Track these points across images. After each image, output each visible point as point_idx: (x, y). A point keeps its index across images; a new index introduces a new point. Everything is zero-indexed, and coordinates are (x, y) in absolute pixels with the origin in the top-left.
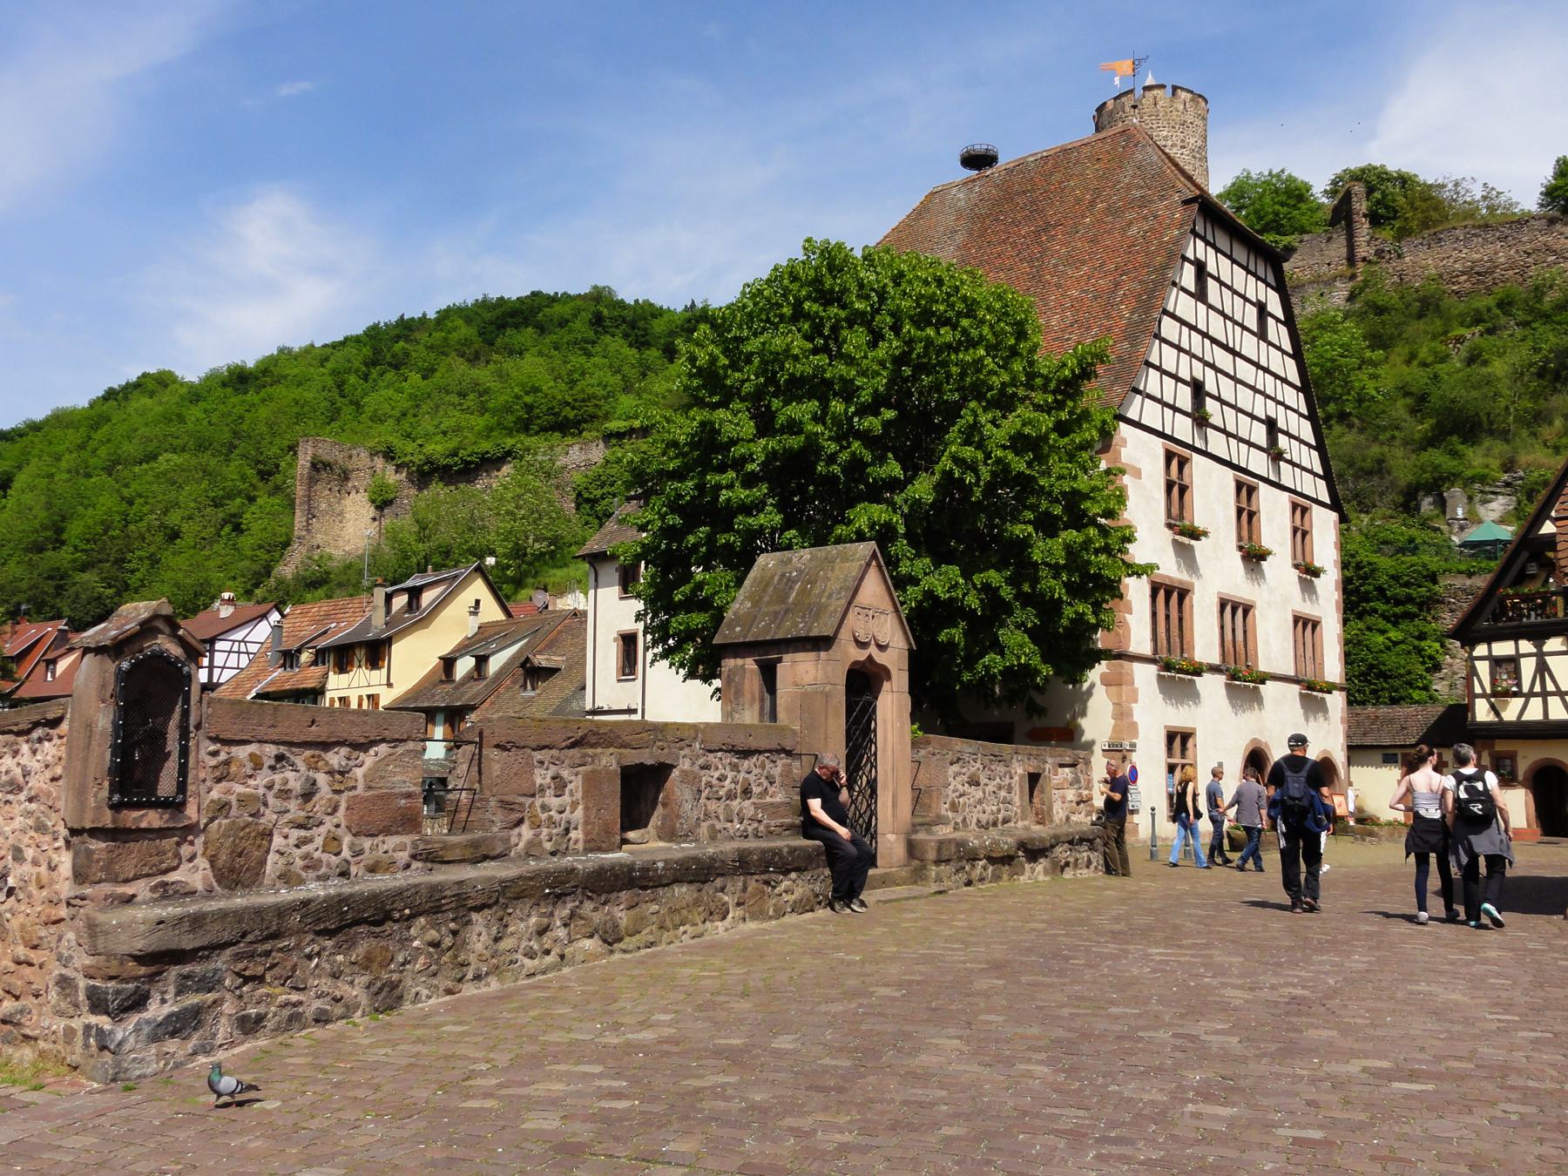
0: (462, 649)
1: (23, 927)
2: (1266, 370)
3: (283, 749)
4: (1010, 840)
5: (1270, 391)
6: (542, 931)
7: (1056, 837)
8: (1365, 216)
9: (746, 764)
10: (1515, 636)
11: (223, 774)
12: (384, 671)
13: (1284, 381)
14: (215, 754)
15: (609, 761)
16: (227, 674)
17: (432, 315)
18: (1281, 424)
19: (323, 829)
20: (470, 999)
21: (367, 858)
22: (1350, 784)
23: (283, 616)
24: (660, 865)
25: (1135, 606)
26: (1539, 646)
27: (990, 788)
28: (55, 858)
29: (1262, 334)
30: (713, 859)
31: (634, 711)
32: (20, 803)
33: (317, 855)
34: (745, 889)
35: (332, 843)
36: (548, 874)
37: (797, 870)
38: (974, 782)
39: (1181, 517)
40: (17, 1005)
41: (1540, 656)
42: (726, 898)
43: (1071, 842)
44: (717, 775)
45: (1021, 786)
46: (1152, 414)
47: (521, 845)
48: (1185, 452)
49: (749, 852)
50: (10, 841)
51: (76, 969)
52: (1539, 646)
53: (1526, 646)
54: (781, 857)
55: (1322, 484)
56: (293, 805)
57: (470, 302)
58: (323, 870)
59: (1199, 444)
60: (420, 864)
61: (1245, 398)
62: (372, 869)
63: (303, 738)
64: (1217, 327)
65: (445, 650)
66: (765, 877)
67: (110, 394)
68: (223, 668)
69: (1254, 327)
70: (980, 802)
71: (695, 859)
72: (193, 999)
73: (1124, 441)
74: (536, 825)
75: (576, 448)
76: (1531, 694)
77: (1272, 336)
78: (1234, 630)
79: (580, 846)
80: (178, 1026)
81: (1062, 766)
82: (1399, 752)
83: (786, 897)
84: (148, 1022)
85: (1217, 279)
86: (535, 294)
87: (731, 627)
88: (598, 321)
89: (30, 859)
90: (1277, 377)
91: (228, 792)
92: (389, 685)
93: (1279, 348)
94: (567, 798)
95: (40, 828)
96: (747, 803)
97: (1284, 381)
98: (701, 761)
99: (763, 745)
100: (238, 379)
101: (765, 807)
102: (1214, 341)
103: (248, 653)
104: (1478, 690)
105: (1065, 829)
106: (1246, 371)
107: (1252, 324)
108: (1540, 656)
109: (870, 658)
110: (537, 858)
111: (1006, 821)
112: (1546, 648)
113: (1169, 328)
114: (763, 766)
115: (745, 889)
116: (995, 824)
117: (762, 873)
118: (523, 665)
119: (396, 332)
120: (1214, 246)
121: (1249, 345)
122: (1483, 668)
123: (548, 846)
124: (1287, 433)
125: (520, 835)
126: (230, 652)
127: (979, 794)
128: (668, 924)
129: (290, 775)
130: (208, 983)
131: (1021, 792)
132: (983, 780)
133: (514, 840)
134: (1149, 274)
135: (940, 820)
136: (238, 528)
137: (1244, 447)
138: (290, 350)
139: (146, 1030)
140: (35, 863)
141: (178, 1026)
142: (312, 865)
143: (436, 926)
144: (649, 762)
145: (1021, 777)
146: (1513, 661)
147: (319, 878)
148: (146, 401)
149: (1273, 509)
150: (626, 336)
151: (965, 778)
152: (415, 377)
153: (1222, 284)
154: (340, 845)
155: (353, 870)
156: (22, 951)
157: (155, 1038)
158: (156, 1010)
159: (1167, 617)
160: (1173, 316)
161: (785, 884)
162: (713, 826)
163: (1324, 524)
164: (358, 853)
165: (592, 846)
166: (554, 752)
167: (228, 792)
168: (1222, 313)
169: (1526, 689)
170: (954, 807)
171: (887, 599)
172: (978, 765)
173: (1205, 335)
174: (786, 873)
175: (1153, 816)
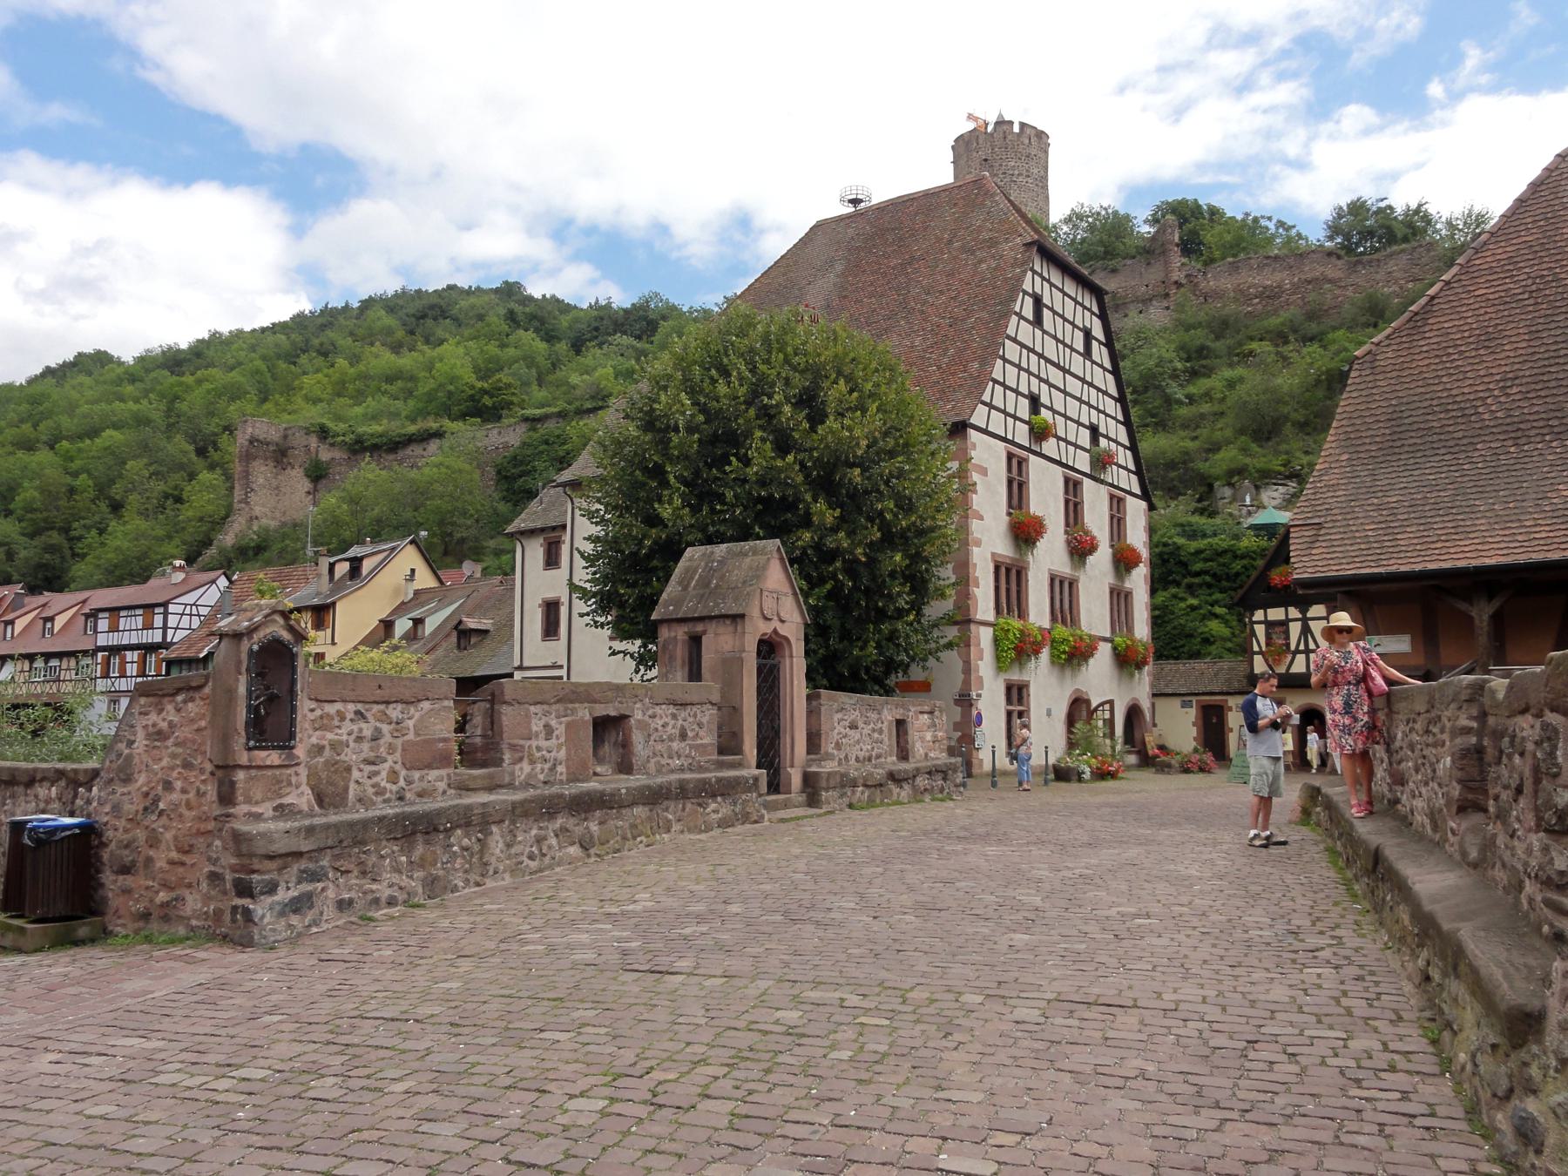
0: (401, 609)
1: (176, 838)
2: (1091, 385)
3: (360, 707)
4: (881, 771)
5: (1093, 402)
6: (539, 840)
7: (918, 769)
8: (1177, 245)
9: (683, 714)
10: (1285, 605)
11: (323, 724)
12: (329, 631)
13: (1105, 393)
14: (312, 710)
15: (585, 713)
16: (180, 635)
17: (356, 305)
18: (1102, 430)
19: (386, 766)
20: (493, 889)
21: (417, 786)
22: (1155, 725)
23: (231, 582)
24: (623, 791)
25: (981, 582)
26: (1304, 611)
27: (866, 731)
28: (203, 788)
29: (1087, 353)
30: (661, 787)
31: (561, 667)
32: (167, 747)
33: (383, 784)
34: (684, 809)
35: (393, 776)
36: (544, 798)
37: (722, 795)
38: (853, 726)
39: (1020, 507)
40: (173, 895)
41: (1305, 621)
42: (670, 817)
43: (929, 773)
44: (660, 723)
45: (890, 730)
46: (997, 423)
47: (523, 777)
48: (1024, 454)
49: (688, 781)
50: (159, 776)
51: (223, 867)
52: (1304, 611)
53: (1294, 612)
54: (710, 785)
55: (1134, 478)
56: (366, 746)
57: (390, 293)
58: (388, 795)
59: (1035, 448)
60: (453, 791)
61: (1073, 408)
62: (420, 795)
63: (372, 699)
64: (1051, 349)
65: (384, 614)
66: (700, 800)
67: (48, 371)
68: (176, 629)
69: (1081, 349)
70: (858, 742)
71: (649, 787)
72: (306, 887)
73: (974, 446)
74: (532, 762)
75: (495, 432)
76: (1297, 651)
77: (1096, 357)
78: (1061, 600)
79: (564, 777)
80: (298, 905)
81: (921, 713)
82: (1194, 699)
83: (714, 816)
84: (278, 903)
85: (1051, 309)
86: (451, 288)
87: (666, 606)
88: (511, 317)
89: (178, 788)
90: (1099, 390)
91: (323, 738)
92: (333, 643)
93: (1101, 366)
94: (554, 741)
95: (187, 765)
96: (683, 745)
97: (1105, 393)
98: (650, 712)
99: (695, 699)
100: (173, 361)
101: (697, 747)
102: (1048, 361)
103: (199, 615)
104: (1256, 648)
105: (924, 764)
106: (1074, 386)
107: (1079, 345)
108: (1305, 621)
109: (775, 631)
110: (534, 787)
111: (878, 757)
112: (1309, 615)
113: (1011, 351)
114: (695, 716)
115: (684, 809)
116: (870, 759)
117: (697, 797)
118: (456, 628)
119: (320, 321)
120: (1048, 281)
121: (1077, 363)
122: (1260, 630)
123: (541, 777)
124: (1106, 437)
125: (521, 769)
126: (182, 614)
127: (857, 736)
128: (629, 835)
129: (364, 725)
130: (314, 877)
131: (890, 735)
132: (861, 725)
133: (517, 773)
134: (995, 305)
135: (829, 757)
136: (179, 500)
137: (1071, 449)
138: (221, 334)
139: (278, 908)
140: (184, 791)
141: (298, 905)
142: (380, 792)
143: (467, 835)
144: (613, 714)
145: (891, 722)
146: (1284, 624)
147: (385, 801)
148: (83, 378)
149: (1095, 501)
150: (537, 331)
151: (847, 724)
152: (341, 362)
153: (1055, 313)
154: (398, 778)
155: (408, 795)
156: (174, 855)
157: (282, 914)
158: (282, 895)
159: (1008, 590)
160: (1014, 340)
161: (713, 806)
162: (659, 762)
163: (1136, 510)
164: (409, 782)
165: (573, 778)
166: (545, 707)
167: (323, 738)
168: (1055, 337)
169: (1293, 647)
170: (838, 746)
171: (787, 585)
172: (857, 713)
173: (1041, 356)
174: (714, 796)
175: (994, 752)
